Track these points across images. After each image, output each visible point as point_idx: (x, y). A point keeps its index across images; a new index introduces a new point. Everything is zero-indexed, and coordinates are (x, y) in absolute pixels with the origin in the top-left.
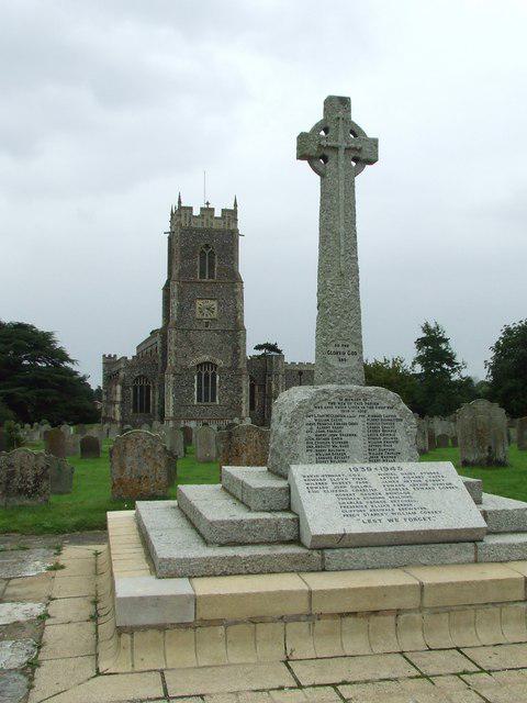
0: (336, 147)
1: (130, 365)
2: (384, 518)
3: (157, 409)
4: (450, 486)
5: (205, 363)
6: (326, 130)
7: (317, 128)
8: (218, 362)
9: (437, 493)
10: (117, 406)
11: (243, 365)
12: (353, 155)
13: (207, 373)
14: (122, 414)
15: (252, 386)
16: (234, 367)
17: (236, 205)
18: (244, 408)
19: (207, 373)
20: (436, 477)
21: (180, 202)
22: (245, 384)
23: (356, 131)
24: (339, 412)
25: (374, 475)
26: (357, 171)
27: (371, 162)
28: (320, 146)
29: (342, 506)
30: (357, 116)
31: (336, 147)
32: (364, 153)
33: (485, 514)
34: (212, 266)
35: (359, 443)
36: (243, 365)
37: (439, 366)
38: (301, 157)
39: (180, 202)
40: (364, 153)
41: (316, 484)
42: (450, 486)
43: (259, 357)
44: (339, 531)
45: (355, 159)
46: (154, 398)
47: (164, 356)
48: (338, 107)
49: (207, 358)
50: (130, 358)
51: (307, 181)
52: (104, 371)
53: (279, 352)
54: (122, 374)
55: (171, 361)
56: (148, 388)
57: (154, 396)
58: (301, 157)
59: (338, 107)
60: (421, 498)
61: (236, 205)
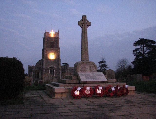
0: (84, 23)
1: (24, 72)
2: (92, 80)
3: (41, 77)
4: (102, 76)
5: (52, 67)
6: (83, 21)
7: (81, 20)
8: (54, 67)
9: (100, 76)
10: (32, 77)
11: (60, 67)
12: (87, 25)
13: (52, 69)
14: (33, 79)
15: (62, 73)
16: (58, 68)
17: (58, 31)
18: (60, 77)
19: (52, 69)
20: (100, 75)
21: (46, 31)
22: (61, 72)
23: (87, 21)
24: (85, 65)
25: (91, 74)
26: (88, 27)
27: (90, 26)
28: (82, 23)
29: (86, 78)
30: (87, 18)
31: (84, 23)
32: (89, 24)
33: (107, 80)
34: (53, 45)
35: (88, 70)
36: (60, 67)
37: (104, 68)
38: (78, 25)
39: (46, 31)
40: (89, 24)
41: (83, 75)
42: (102, 76)
43: (64, 66)
44: (86, 81)
45: (87, 25)
46: (40, 75)
47: (42, 65)
48: (84, 17)
49: (52, 66)
50: (35, 66)
51: (80, 29)
52: (29, 69)
53: (68, 65)
54: (33, 69)
55: (44, 67)
56: (39, 72)
57: (40, 75)
58: (78, 25)
59: (84, 17)
60: (98, 77)
61: (58, 31)
